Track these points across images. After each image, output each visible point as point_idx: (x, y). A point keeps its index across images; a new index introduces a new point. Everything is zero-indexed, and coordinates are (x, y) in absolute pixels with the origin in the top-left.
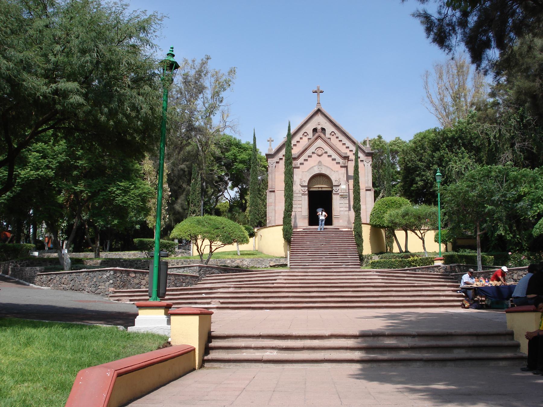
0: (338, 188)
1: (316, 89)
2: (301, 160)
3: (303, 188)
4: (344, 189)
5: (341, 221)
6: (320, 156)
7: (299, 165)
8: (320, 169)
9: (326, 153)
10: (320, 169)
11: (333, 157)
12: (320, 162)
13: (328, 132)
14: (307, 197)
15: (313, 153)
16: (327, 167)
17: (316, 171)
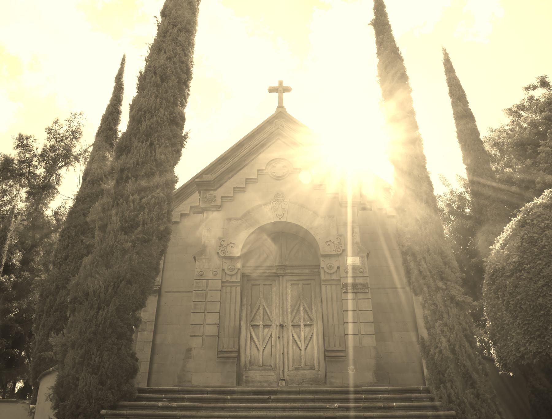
0: (335, 263)
1: (276, 85)
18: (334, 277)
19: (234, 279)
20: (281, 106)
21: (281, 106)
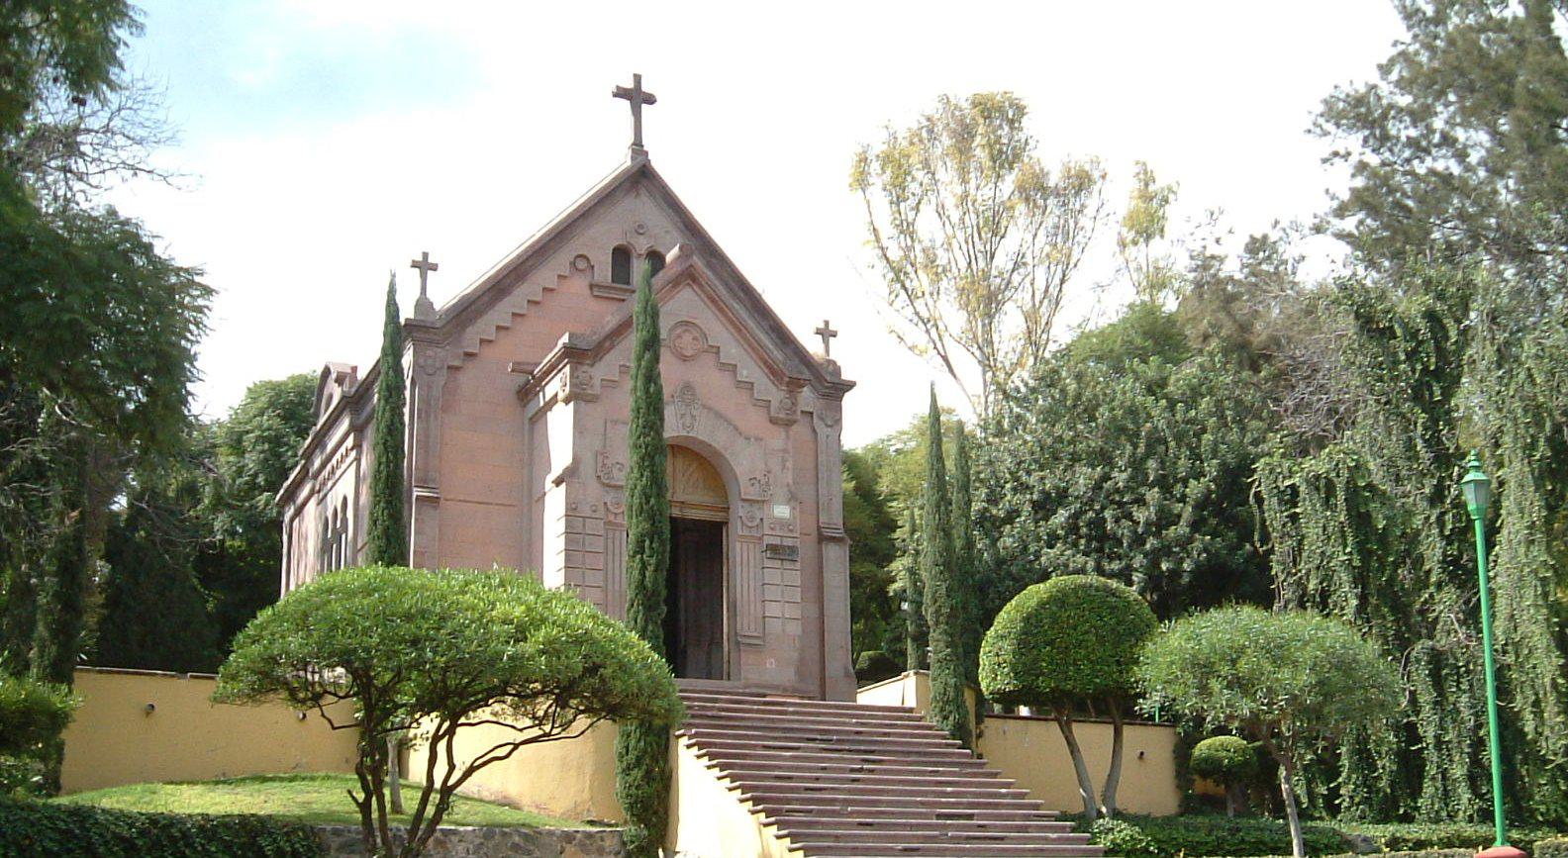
1: (629, 84)
4: (781, 523)
5: (771, 664)
7: (597, 390)
11: (744, 374)
16: (719, 415)
18: (754, 533)
19: (619, 520)
20: (638, 147)
21: (638, 147)
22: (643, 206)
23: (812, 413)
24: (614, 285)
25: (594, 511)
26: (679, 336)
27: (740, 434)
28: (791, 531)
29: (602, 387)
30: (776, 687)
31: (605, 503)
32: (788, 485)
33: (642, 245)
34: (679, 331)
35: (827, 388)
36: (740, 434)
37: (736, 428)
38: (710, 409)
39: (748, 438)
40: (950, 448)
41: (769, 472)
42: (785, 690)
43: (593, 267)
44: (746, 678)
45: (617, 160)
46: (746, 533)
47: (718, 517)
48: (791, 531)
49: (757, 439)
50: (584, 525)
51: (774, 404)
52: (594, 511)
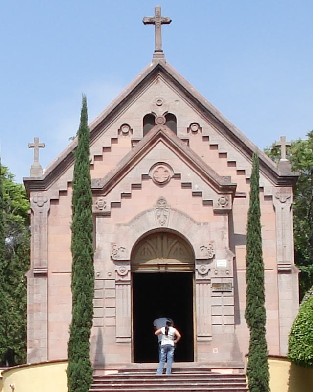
2: (114, 195)
3: (118, 268)
4: (222, 269)
5: (215, 351)
6: (161, 184)
8: (162, 218)
9: (178, 176)
10: (162, 218)
11: (196, 187)
12: (161, 200)
13: (182, 123)
14: (128, 289)
15: (145, 177)
16: (181, 213)
17: (153, 223)
18: (206, 278)
19: (125, 279)
22: (160, 89)
23: (272, 196)
24: (159, 133)
25: (110, 276)
26: (156, 171)
27: (195, 222)
28: (228, 274)
29: (112, 207)
30: (218, 364)
31: (116, 271)
32: (226, 248)
33: (160, 112)
34: (156, 168)
35: (279, 179)
36: (195, 222)
37: (191, 219)
38: (175, 210)
39: (199, 224)
40: (153, 253)
41: (212, 242)
42: (224, 365)
43: (132, 130)
44: (200, 360)
45: (152, 65)
46: (201, 278)
47: (187, 269)
48: (228, 274)
49: (204, 224)
50: (104, 284)
51: (215, 202)
52: (110, 276)
